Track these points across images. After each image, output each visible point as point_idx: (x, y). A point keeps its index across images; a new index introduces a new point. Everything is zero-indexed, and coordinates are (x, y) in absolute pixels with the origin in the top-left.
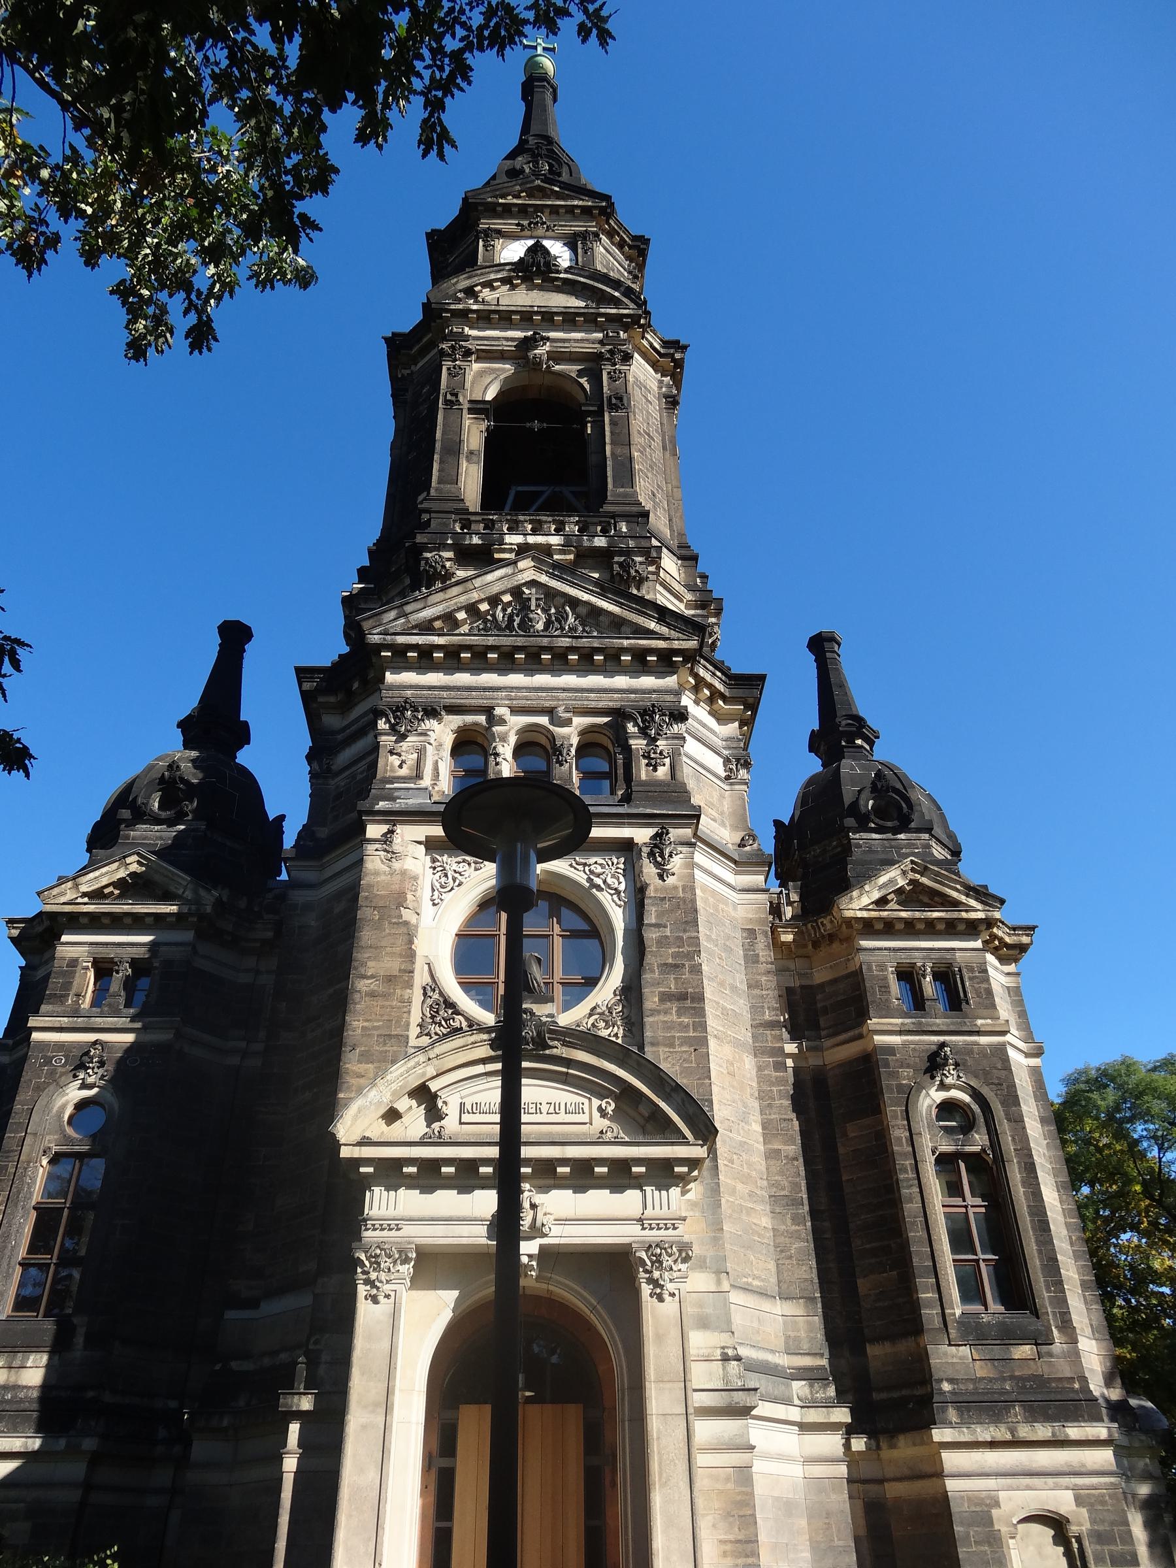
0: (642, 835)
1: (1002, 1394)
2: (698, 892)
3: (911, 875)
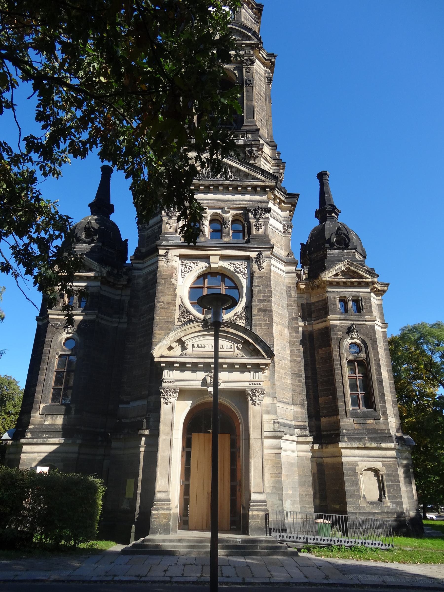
0: (253, 254)
1: (362, 434)
2: (272, 274)
3: (347, 266)
